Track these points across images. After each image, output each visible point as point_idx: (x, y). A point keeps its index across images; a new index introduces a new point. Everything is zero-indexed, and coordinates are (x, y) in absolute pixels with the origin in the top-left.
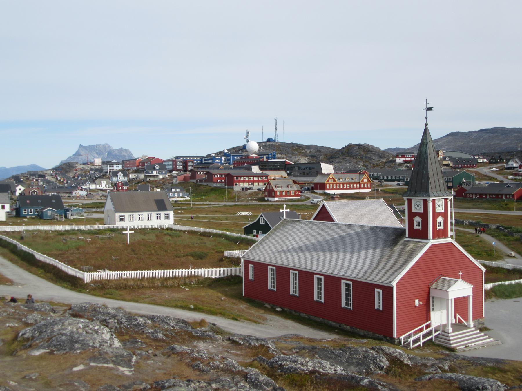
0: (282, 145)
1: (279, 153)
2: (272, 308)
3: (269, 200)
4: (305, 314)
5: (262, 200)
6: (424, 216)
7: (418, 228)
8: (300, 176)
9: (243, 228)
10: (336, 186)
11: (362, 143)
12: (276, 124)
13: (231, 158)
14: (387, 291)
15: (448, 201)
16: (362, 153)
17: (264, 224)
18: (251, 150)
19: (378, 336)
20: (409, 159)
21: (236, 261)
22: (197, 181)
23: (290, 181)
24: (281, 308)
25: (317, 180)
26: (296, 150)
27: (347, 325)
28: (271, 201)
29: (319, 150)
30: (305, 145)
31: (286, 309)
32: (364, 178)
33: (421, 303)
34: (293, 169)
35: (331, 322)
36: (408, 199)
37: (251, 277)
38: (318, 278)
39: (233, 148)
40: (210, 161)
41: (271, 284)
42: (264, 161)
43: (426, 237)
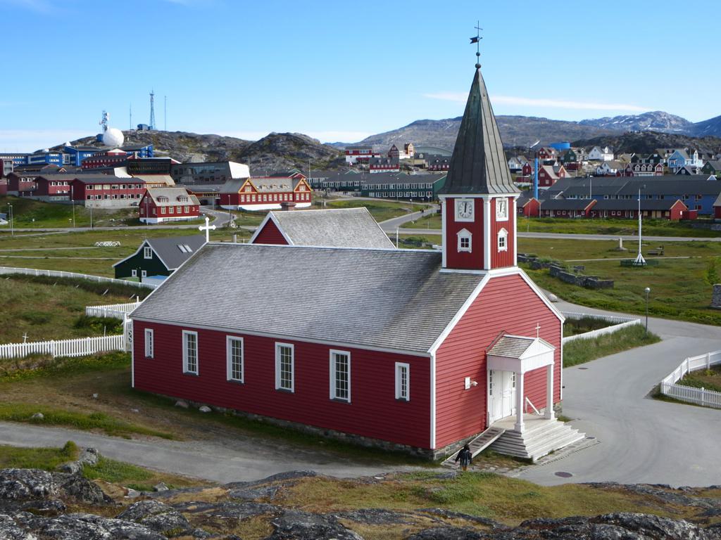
0: (161, 134)
1: (158, 148)
2: (191, 406)
3: (147, 222)
4: (256, 416)
5: (136, 222)
6: (476, 228)
7: (465, 249)
8: (196, 184)
9: (113, 266)
10: (257, 199)
11: (292, 132)
12: (152, 101)
13: (77, 155)
14: (420, 366)
15: (514, 201)
16: (293, 148)
17: (151, 258)
18: (111, 139)
19: (401, 448)
20: (365, 156)
21: (112, 325)
22: (20, 193)
23: (182, 191)
24: (211, 408)
25: (225, 188)
26: (186, 143)
27: (340, 432)
28: (150, 224)
29: (222, 142)
30: (200, 135)
31: (219, 408)
32: (301, 185)
33: (476, 383)
34: (184, 172)
35: (308, 427)
36: (447, 199)
37: (149, 351)
38: (233, 341)
39: (80, 141)
40: (40, 161)
41: (189, 363)
42: (133, 159)
43: (480, 266)
